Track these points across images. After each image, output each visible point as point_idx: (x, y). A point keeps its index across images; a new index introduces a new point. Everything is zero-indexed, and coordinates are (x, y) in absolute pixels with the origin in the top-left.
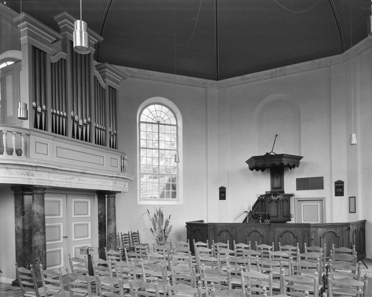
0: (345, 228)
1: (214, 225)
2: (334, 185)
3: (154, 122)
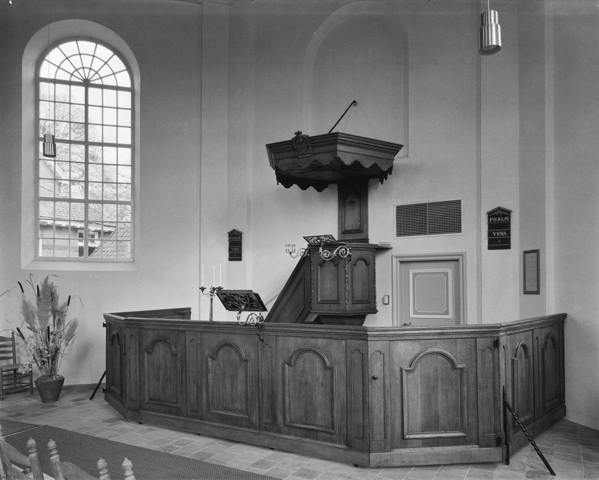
0: (482, 343)
2: (487, 220)
3: (74, 79)
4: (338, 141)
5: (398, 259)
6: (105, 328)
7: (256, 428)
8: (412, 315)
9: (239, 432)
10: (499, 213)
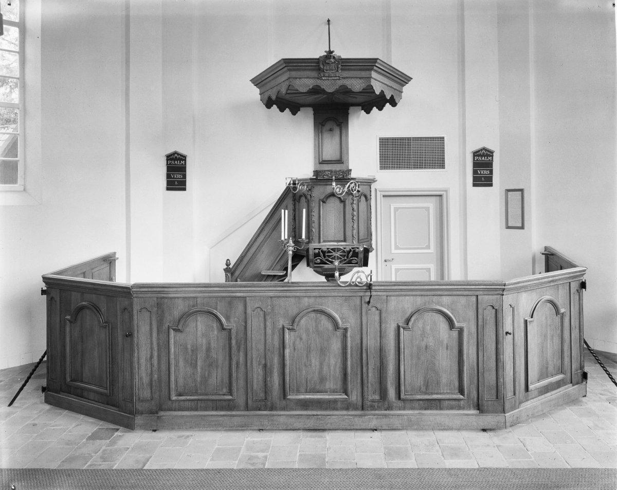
1: (159, 292)
2: (166, 162)
4: (375, 68)
5: (381, 193)
6: (45, 296)
7: (356, 409)
8: (394, 251)
9: (333, 417)
10: (484, 153)
